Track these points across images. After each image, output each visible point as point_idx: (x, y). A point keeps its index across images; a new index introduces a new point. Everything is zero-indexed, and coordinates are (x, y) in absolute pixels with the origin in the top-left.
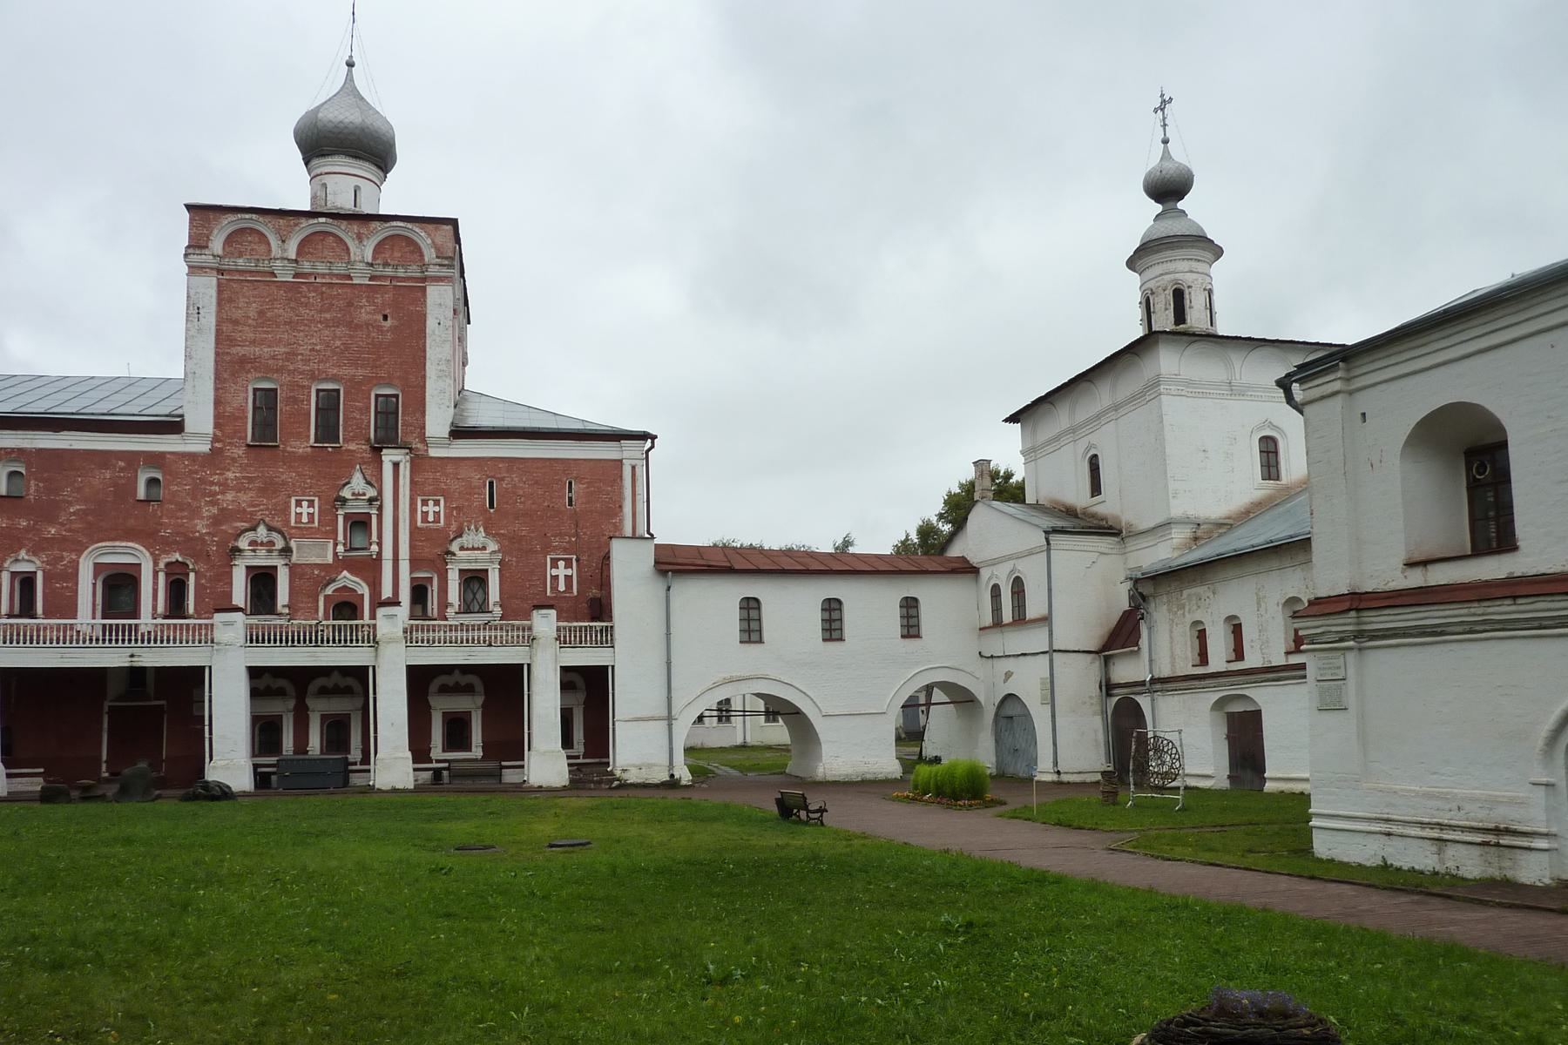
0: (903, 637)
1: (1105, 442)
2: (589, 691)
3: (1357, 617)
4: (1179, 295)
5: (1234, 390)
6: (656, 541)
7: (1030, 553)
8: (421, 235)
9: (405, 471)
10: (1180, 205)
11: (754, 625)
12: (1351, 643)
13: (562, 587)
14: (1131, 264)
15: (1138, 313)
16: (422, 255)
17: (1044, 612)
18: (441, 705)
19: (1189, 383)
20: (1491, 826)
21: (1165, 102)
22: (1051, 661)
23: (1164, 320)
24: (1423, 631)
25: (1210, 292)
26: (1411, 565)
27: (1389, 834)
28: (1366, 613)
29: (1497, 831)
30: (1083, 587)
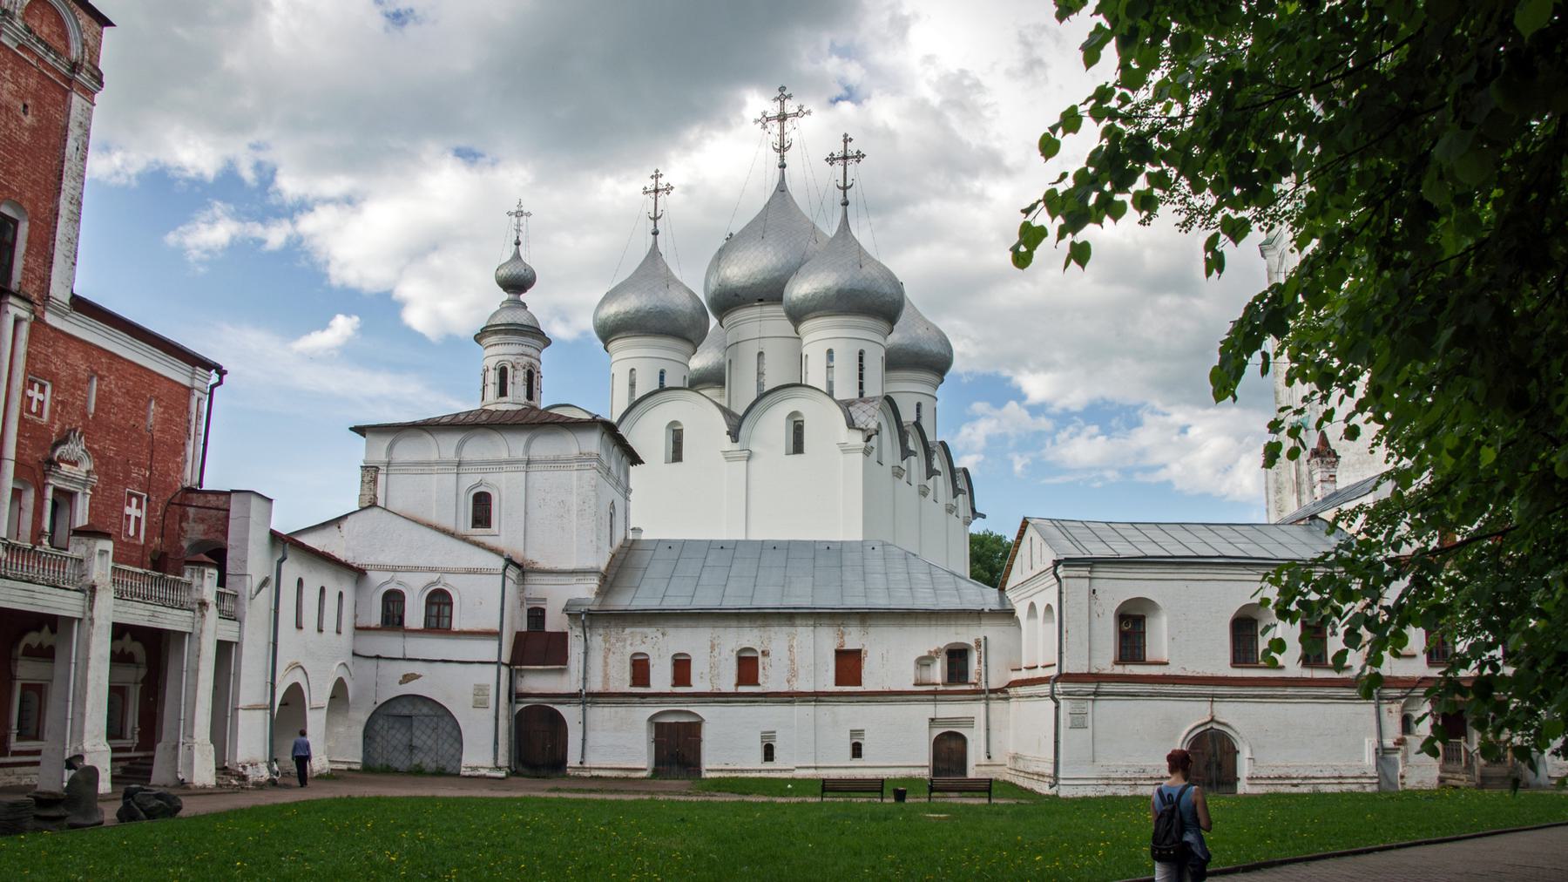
7: (585, 572)
9: (24, 329)
10: (523, 297)
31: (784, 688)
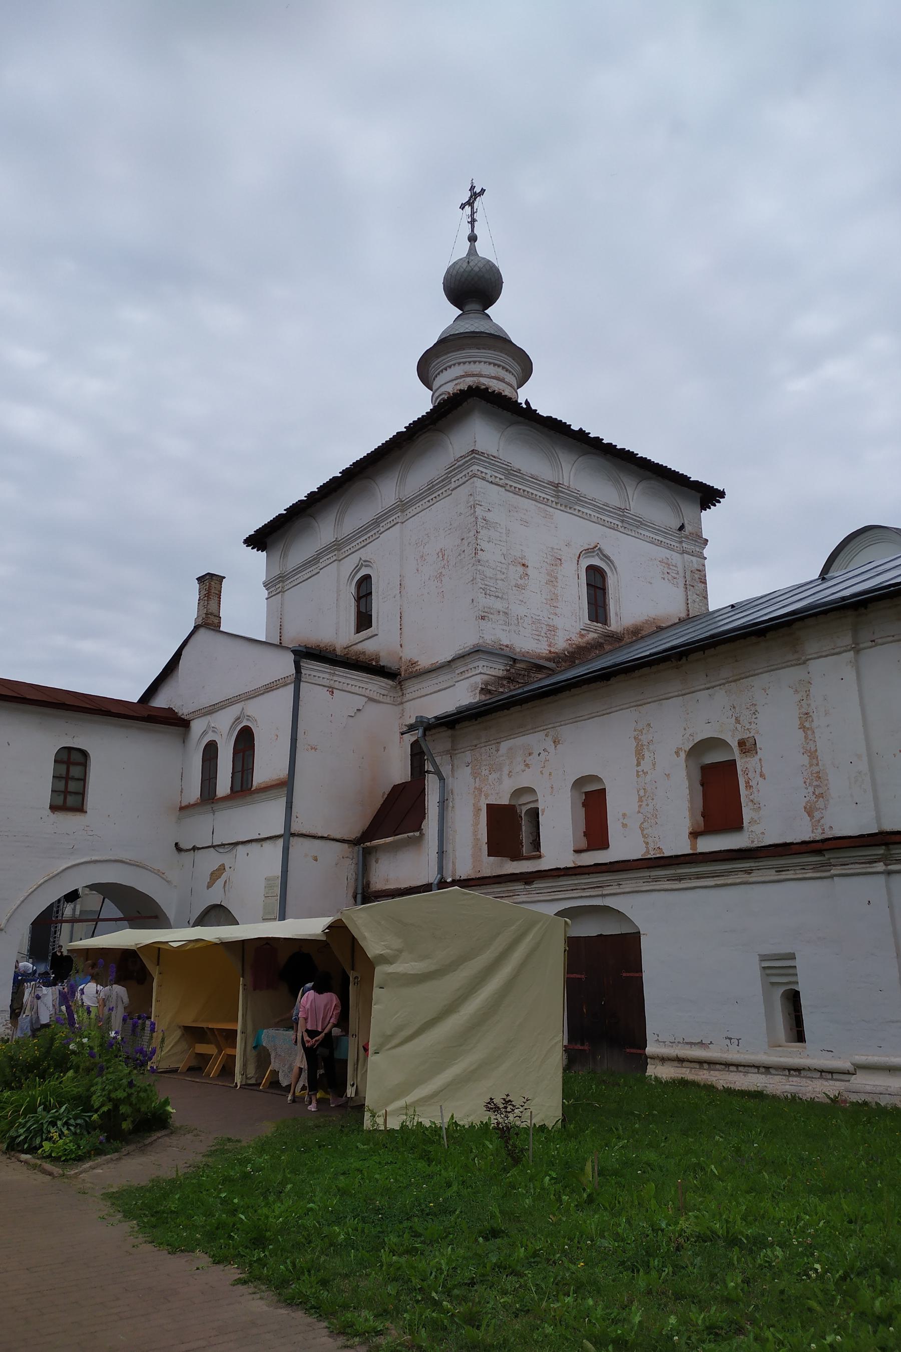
0: (54, 808)
7: (270, 688)
19: (511, 472)
21: (475, 195)
31: (802, 832)
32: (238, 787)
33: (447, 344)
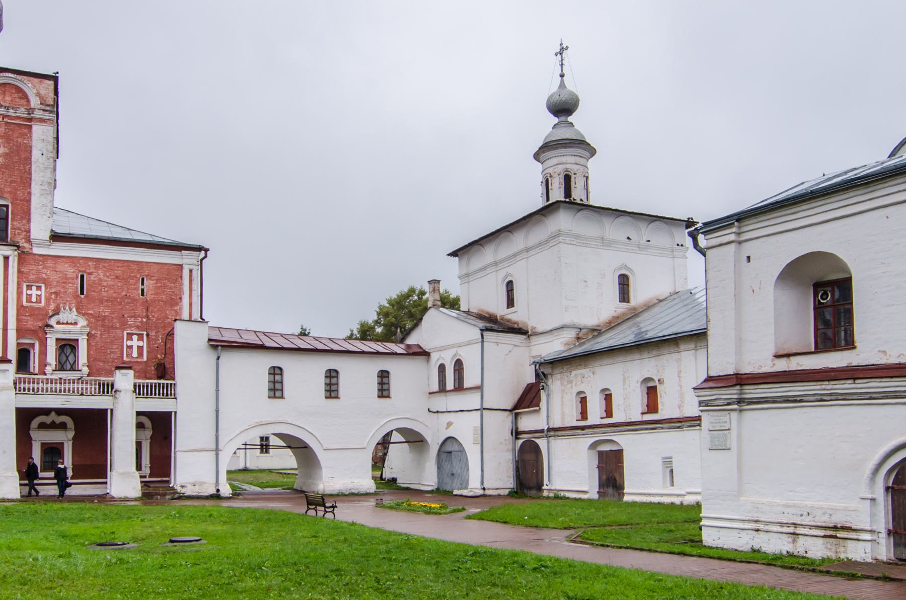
0: (379, 397)
1: (518, 272)
2: (158, 429)
3: (736, 388)
4: (567, 179)
5: (605, 243)
6: (210, 324)
7: (469, 343)
8: (29, 87)
10: (570, 119)
11: (278, 386)
12: (735, 407)
13: (135, 354)
14: (537, 156)
15: (540, 190)
16: (28, 101)
17: (478, 383)
18: (39, 438)
19: (577, 237)
20: (831, 525)
21: (562, 50)
22: (482, 415)
23: (557, 194)
24: (786, 400)
25: (587, 178)
26: (778, 356)
27: (757, 530)
28: (746, 387)
29: (835, 528)
30: (504, 366)
31: (676, 414)
32: (457, 386)
33: (547, 147)
